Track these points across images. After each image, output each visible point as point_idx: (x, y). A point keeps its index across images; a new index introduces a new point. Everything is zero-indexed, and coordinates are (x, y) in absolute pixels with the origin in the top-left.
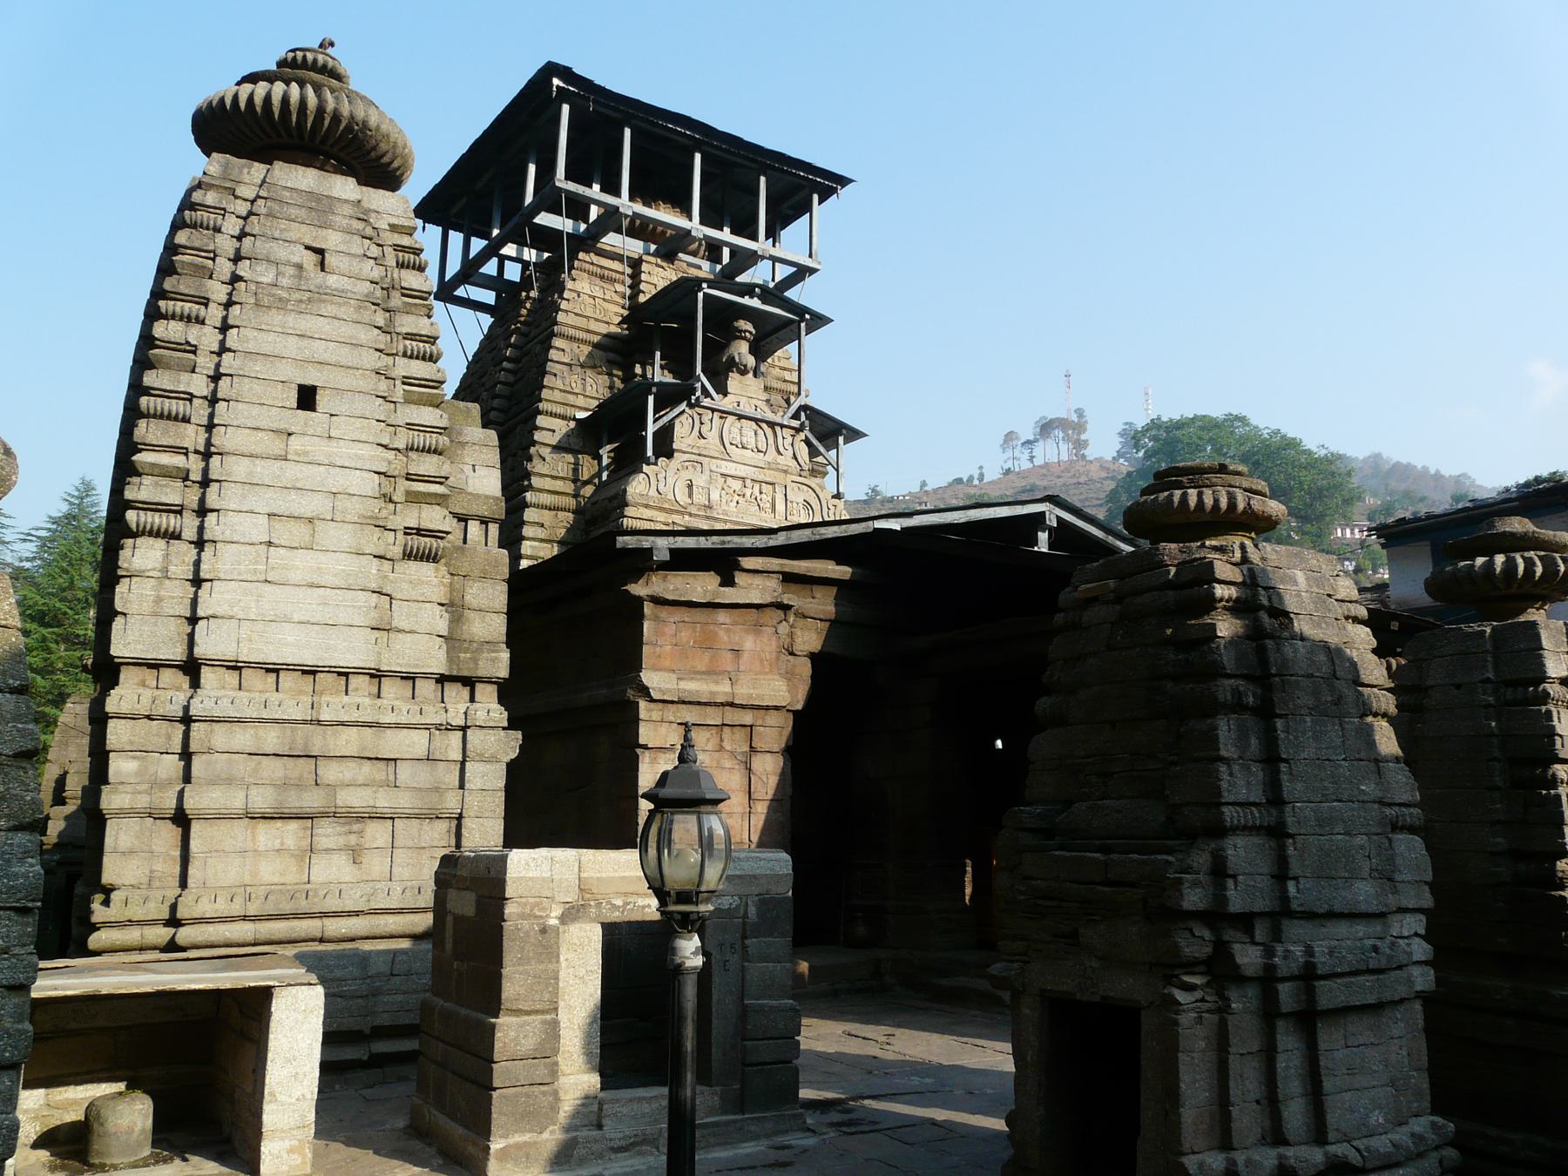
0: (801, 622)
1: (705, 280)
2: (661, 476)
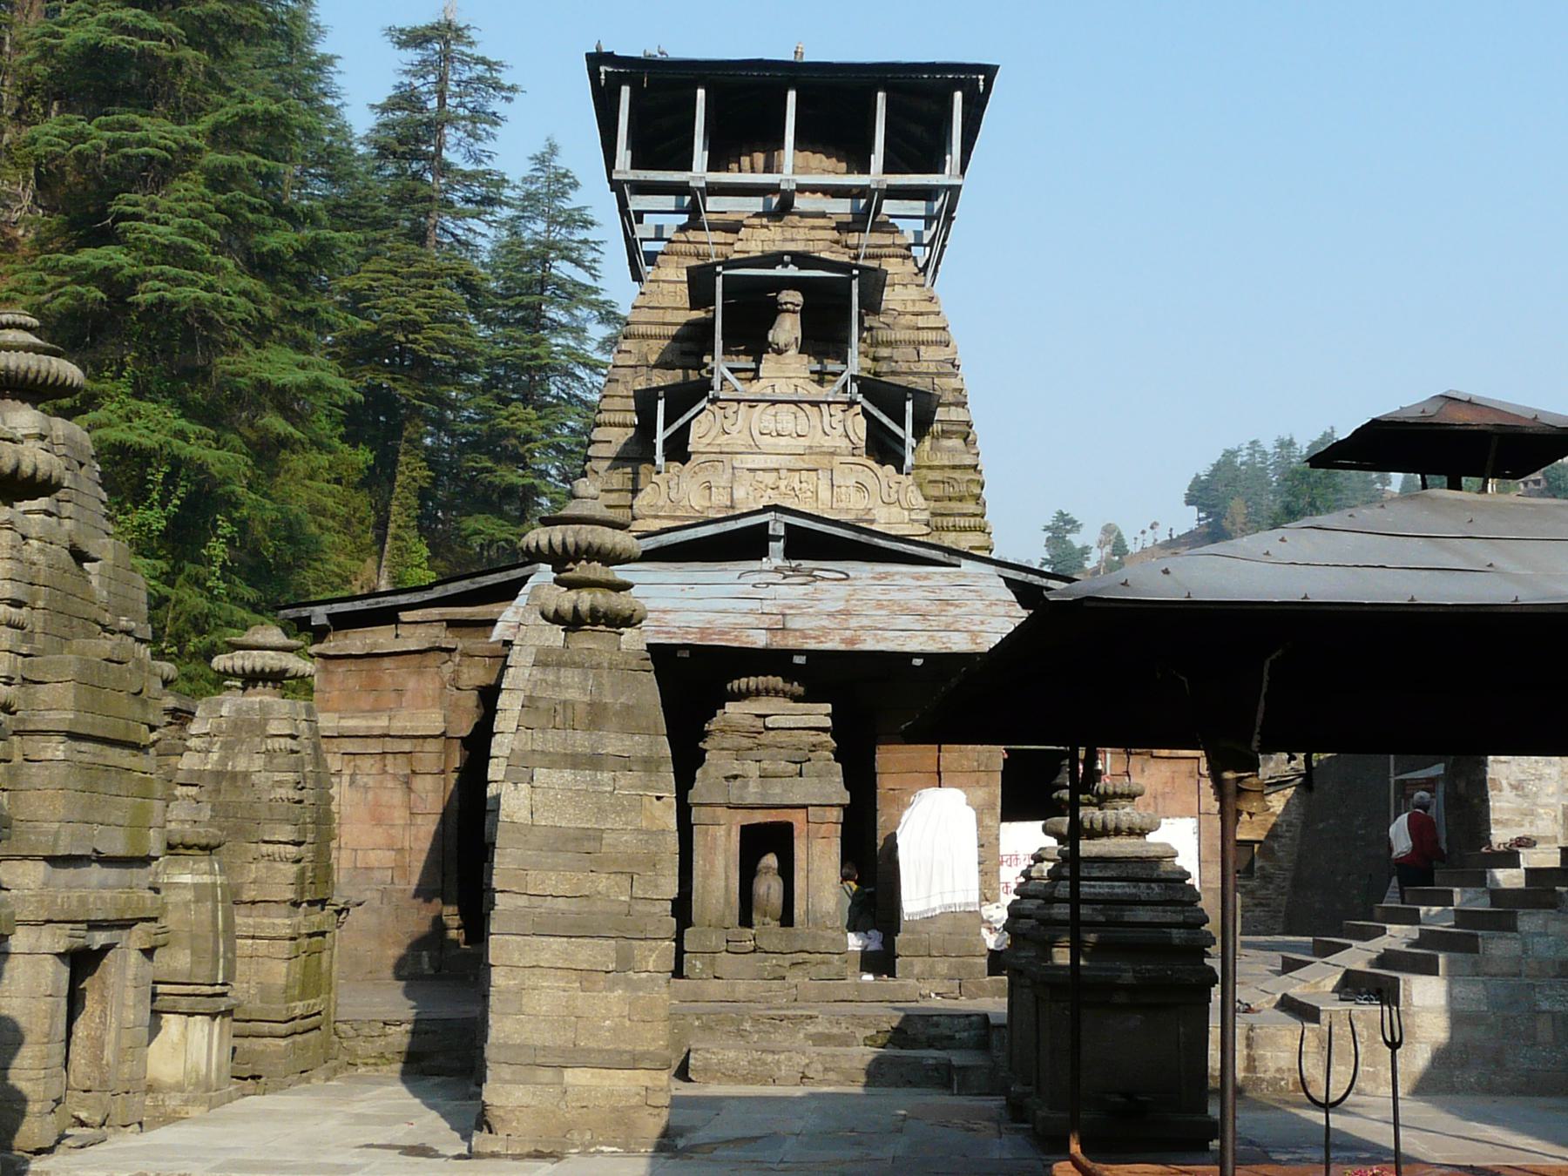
0: (467, 661)
1: (719, 264)
2: (672, 484)
